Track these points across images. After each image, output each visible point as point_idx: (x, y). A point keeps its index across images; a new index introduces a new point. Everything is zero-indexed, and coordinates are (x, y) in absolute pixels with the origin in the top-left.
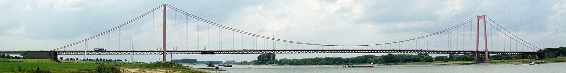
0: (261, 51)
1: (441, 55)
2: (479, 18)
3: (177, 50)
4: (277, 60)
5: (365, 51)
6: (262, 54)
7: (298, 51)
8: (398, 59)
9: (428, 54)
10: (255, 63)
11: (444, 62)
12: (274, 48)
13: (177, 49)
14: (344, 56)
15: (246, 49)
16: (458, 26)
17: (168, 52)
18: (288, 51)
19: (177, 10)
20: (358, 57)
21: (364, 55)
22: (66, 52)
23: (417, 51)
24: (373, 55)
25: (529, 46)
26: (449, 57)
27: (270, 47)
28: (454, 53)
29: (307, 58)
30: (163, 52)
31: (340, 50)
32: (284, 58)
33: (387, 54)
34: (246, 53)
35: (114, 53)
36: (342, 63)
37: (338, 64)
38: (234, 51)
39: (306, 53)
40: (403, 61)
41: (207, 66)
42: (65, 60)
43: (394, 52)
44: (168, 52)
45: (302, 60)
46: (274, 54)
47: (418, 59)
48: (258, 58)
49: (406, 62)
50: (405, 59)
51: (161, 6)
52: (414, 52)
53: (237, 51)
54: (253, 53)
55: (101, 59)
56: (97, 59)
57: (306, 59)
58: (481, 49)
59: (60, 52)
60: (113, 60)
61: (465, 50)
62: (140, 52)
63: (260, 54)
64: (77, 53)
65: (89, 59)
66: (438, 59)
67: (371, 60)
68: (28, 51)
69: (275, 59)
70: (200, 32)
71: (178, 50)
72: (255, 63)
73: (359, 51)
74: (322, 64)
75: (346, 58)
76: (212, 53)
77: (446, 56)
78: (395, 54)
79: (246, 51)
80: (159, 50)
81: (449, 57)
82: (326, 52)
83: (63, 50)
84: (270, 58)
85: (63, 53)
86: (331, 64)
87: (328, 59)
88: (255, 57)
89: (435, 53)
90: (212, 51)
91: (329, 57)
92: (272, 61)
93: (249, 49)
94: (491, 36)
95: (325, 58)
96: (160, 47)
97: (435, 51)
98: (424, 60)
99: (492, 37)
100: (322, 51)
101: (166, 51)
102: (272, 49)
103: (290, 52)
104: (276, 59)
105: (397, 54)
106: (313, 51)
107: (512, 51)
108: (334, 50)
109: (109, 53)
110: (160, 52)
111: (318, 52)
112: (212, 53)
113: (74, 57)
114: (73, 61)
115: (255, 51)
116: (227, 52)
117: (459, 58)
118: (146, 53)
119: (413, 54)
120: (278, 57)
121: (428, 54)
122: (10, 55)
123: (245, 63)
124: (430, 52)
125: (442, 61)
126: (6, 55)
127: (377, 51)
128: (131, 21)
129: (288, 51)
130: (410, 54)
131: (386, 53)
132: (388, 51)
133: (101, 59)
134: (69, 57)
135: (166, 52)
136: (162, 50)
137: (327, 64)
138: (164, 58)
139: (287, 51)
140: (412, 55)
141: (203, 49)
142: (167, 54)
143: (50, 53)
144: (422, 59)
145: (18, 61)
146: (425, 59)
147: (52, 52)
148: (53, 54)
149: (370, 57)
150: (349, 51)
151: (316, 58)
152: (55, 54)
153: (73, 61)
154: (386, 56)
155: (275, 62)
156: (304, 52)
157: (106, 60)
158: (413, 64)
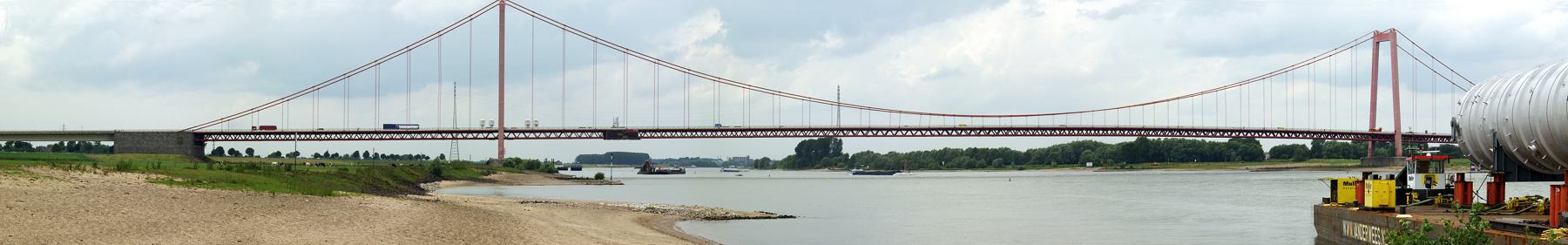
0: (802, 130)
1: (1289, 142)
2: (1379, 38)
3: (536, 128)
4: (847, 155)
5: (1099, 129)
6: (807, 139)
7: (920, 130)
8: (1166, 154)
9: (1257, 139)
10: (791, 164)
11: (1294, 161)
12: (470, 125)
13: (536, 125)
14: (1020, 144)
15: (725, 124)
16: (1316, 59)
17: (510, 132)
18: (894, 129)
19: (442, 33)
20: (1054, 148)
22: (227, 135)
23: (1308, 132)
24: (1098, 141)
26: (1310, 147)
27: (824, 118)
28: (1324, 139)
29: (923, 150)
31: (1028, 127)
32: (865, 150)
33: (1133, 139)
34: (367, 137)
35: (434, 135)
36: (1009, 164)
37: (999, 167)
38: (752, 130)
39: (940, 135)
40: (1180, 157)
41: (639, 173)
42: (269, 156)
43: (1194, 134)
44: (510, 132)
45: (1029, 154)
46: (839, 138)
47: (1221, 153)
48: (797, 149)
49: (1187, 161)
50: (1186, 152)
53: (758, 130)
54: (802, 134)
55: (366, 154)
56: (356, 154)
57: (919, 153)
58: (1386, 125)
59: (210, 134)
60: (341, 154)
61: (1354, 129)
62: (558, 131)
63: (803, 139)
64: (318, 136)
65: (331, 153)
66: (1279, 154)
67: (1089, 155)
68: (119, 132)
69: (841, 154)
70: (1456, 95)
71: (541, 127)
72: (791, 164)
73: (1082, 129)
74: (959, 167)
75: (1000, 149)
76: (632, 135)
77: (1304, 145)
78: (1156, 138)
79: (722, 131)
80: (487, 126)
81: (1310, 147)
82: (1010, 133)
83: (225, 127)
84: (829, 149)
85: (278, 136)
86: (982, 167)
87: (974, 152)
88: (786, 147)
89: (1301, 136)
90: (631, 130)
91: (978, 147)
92: (832, 158)
93: (732, 126)
94: (595, 62)
95: (967, 150)
96: (490, 118)
97: (1286, 132)
98: (1238, 155)
99: (599, 66)
100: (981, 129)
101: (505, 131)
102: (835, 125)
103: (909, 133)
104: (844, 151)
105: (1162, 139)
106: (959, 132)
107: (1246, 126)
108: (1014, 129)
109: (408, 137)
110: (489, 132)
111: (982, 133)
112: (632, 135)
114: (238, 160)
115: (807, 130)
116: (328, 136)
117: (1335, 152)
118: (522, 135)
119: (1207, 140)
120: (851, 146)
121: (1257, 139)
122: (102, 143)
123: (763, 164)
124: (1286, 135)
125: (1290, 158)
126: (93, 143)
127: (1114, 131)
128: (408, 49)
129: (894, 129)
130: (1200, 139)
131: (1132, 135)
132: (1137, 129)
133: (366, 154)
134: (321, 147)
135: (506, 134)
136: (496, 126)
137: (971, 167)
138: (502, 152)
139: (891, 130)
140: (1203, 141)
141: (608, 126)
142: (507, 138)
143: (181, 136)
144: (1234, 153)
146: (1241, 152)
147: (188, 133)
148: (191, 139)
149: (1088, 148)
150: (1055, 129)
151: (945, 149)
152: (199, 138)
153: (238, 160)
154: (1131, 144)
155: (840, 161)
156: (945, 133)
157: (383, 156)
158: (600, 177)
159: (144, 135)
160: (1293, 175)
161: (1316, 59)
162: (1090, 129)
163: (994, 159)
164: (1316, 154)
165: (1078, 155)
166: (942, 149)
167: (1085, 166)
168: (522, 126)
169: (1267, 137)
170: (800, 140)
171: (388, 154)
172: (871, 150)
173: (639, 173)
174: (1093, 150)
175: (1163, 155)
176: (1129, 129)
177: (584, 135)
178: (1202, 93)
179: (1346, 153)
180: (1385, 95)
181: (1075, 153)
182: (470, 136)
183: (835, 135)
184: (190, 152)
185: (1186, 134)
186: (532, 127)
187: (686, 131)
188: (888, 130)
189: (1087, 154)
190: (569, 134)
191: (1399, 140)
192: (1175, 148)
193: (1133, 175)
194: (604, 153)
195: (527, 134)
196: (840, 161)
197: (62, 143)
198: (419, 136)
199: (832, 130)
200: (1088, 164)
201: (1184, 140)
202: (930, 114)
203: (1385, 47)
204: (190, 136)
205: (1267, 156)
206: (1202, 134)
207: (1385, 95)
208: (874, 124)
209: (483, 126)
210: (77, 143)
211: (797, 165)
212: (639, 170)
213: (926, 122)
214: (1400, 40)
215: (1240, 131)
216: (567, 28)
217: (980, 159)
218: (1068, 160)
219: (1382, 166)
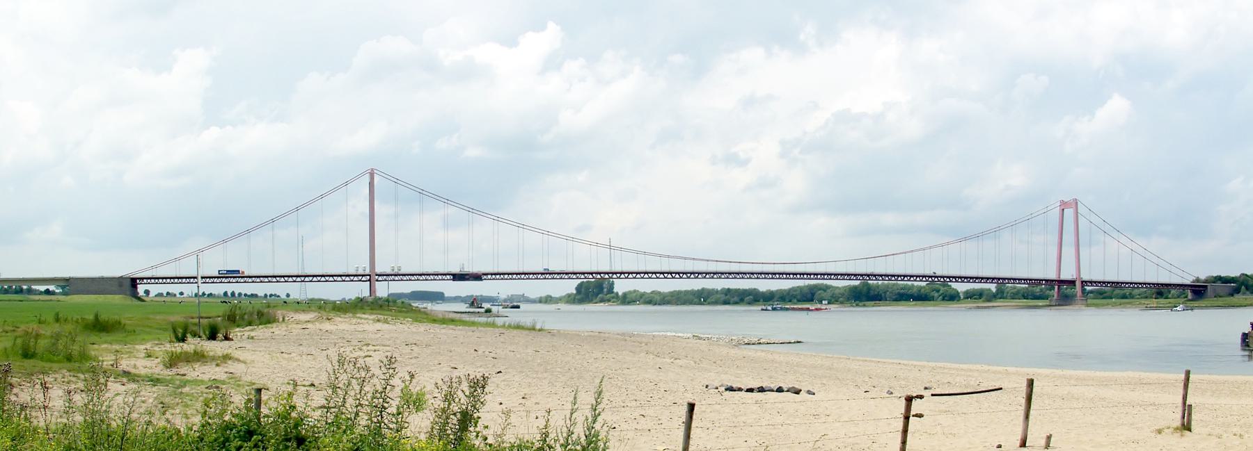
2: (1064, 205)
5: (831, 274)
7: (663, 273)
8: (883, 295)
10: (570, 299)
11: (984, 301)
13: (400, 270)
14: (764, 286)
15: (551, 269)
16: (1017, 222)
17: (379, 275)
19: (399, 182)
20: (793, 289)
21: (806, 284)
25: (1174, 270)
30: (368, 277)
32: (632, 289)
33: (857, 283)
36: (759, 301)
41: (467, 308)
44: (379, 275)
48: (577, 289)
51: (358, 177)
52: (900, 279)
55: (233, 294)
57: (680, 292)
66: (970, 295)
68: (72, 278)
69: (613, 292)
71: (403, 271)
72: (570, 299)
74: (716, 303)
75: (777, 291)
76: (477, 277)
78: (876, 282)
88: (570, 286)
93: (557, 270)
95: (721, 290)
96: (363, 266)
104: (615, 290)
105: (880, 282)
109: (574, 277)
110: (363, 276)
111: (715, 276)
112: (477, 277)
113: (175, 289)
114: (173, 299)
120: (621, 286)
124: (954, 280)
127: (837, 276)
133: (233, 294)
135: (377, 277)
136: (367, 272)
140: (913, 285)
141: (456, 270)
142: (377, 281)
145: (51, 300)
147: (126, 278)
148: (128, 283)
149: (820, 289)
151: (703, 289)
152: (134, 282)
154: (855, 287)
155: (613, 298)
156: (670, 276)
157: (245, 295)
159: (93, 280)
160: (900, 308)
161: (1017, 222)
162: (824, 274)
163: (747, 296)
164: (999, 296)
165: (813, 295)
166: (700, 288)
167: (822, 303)
168: (389, 271)
169: (957, 281)
170: (579, 281)
171: (249, 294)
172: (637, 289)
173: (467, 308)
174: (825, 291)
175: (881, 295)
176: (855, 275)
177: (396, 278)
178: (912, 251)
179: (1026, 295)
180: (1069, 252)
181: (812, 294)
182: (290, 279)
183: (610, 278)
184: (128, 293)
185: (874, 278)
186: (396, 271)
187: (495, 274)
188: (977, 278)
189: (820, 294)
190: (360, 278)
191: (1078, 284)
192: (890, 290)
193: (867, 311)
194: (409, 292)
195: (344, 278)
196: (613, 298)
197: (11, 287)
198: (250, 280)
199: (608, 273)
200: (824, 302)
201: (897, 284)
202: (717, 261)
203: (1069, 212)
204: (129, 280)
205: (962, 297)
206: (887, 279)
207: (1069, 252)
208: (696, 269)
209: (364, 270)
210: (14, 287)
211: (576, 301)
212: (468, 305)
213: (712, 267)
214: (1081, 209)
215: (1131, 283)
216: (399, 182)
217: (733, 297)
218: (804, 299)
219: (1066, 305)
